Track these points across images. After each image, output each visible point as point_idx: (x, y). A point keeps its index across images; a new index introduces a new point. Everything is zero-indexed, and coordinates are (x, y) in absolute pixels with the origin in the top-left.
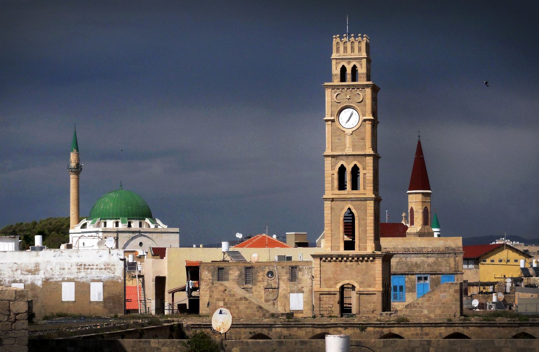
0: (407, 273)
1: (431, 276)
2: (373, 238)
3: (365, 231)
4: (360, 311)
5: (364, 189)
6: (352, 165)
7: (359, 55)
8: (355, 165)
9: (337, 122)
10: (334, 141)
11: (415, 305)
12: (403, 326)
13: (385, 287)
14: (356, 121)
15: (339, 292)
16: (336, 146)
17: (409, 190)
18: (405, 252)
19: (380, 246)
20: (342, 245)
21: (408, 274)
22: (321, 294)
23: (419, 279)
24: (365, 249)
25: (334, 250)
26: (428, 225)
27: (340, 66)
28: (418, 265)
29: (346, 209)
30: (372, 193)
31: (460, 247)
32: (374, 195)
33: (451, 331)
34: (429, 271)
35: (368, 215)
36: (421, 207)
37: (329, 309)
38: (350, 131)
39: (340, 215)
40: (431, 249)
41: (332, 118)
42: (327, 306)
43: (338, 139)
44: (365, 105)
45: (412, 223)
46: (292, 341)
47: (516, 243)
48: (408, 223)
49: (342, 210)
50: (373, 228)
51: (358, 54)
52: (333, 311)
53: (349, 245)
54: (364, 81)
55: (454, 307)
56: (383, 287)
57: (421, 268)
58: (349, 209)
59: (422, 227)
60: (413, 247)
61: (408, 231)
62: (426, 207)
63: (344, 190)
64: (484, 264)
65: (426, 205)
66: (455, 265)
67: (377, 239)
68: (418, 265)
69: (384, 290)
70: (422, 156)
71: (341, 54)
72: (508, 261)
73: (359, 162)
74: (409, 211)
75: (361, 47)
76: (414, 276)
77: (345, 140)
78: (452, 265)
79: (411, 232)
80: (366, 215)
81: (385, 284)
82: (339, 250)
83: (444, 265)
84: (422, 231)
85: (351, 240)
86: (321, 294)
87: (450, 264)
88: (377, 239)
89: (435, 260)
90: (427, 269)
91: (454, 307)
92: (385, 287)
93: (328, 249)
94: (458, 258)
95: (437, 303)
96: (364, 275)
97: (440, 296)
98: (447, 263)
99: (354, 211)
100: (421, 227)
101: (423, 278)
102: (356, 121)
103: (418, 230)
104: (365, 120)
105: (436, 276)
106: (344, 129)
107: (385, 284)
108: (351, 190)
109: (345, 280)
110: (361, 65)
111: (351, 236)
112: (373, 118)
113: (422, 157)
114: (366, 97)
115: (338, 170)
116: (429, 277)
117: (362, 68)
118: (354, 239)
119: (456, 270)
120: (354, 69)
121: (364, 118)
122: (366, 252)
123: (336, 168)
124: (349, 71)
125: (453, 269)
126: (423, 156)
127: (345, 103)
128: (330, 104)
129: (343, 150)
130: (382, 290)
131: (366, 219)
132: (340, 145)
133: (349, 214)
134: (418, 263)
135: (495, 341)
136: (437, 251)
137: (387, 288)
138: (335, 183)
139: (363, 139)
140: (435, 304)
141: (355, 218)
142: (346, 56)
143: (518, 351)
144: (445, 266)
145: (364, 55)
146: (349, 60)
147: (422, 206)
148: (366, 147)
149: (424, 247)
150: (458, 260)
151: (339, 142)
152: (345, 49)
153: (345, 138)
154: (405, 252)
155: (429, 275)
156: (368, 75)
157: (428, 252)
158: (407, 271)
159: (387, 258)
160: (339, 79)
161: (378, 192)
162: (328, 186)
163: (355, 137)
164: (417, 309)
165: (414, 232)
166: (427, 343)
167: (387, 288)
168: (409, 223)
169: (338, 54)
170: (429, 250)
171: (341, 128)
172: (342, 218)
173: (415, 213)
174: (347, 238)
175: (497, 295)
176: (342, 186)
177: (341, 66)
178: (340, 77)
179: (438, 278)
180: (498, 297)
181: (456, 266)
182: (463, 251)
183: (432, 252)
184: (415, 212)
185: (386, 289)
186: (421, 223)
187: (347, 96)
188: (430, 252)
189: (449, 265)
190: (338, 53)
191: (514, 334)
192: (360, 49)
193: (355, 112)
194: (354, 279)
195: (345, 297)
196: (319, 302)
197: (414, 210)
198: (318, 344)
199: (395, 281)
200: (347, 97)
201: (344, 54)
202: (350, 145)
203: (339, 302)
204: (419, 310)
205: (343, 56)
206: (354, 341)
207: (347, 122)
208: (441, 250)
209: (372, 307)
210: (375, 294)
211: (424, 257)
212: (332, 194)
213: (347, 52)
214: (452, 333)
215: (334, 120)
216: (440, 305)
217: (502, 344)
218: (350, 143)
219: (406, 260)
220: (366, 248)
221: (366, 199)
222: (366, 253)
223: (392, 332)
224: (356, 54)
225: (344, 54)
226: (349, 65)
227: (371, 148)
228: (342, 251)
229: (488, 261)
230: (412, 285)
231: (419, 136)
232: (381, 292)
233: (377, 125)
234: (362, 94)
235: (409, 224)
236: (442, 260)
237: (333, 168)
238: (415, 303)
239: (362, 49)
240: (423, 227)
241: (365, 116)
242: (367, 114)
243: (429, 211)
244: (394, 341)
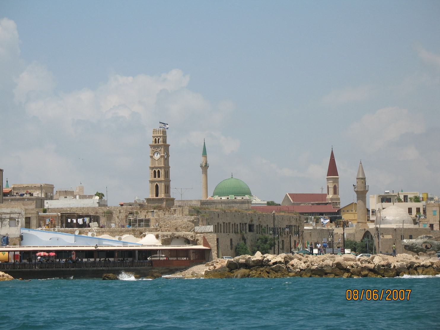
27: (155, 138)
124: (157, 140)
126: (334, 158)
139: (161, 162)
146: (157, 137)
176: (155, 177)
224: (159, 135)
228: (155, 197)
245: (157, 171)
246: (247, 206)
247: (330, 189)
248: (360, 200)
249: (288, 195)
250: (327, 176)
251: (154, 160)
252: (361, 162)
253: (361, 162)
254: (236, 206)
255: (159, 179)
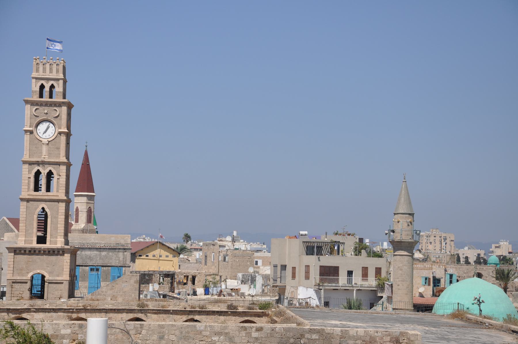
0: (82, 264)
1: (102, 268)
2: (63, 234)
3: (56, 229)
4: (49, 297)
5: (57, 191)
6: (47, 171)
7: (57, 76)
8: (50, 171)
9: (35, 133)
10: (31, 149)
11: (100, 293)
12: (435, 324)
13: (72, 277)
14: (52, 133)
15: (30, 281)
16: (33, 153)
17: (75, 192)
18: (81, 246)
19: (68, 241)
20: (35, 239)
21: (82, 266)
22: (13, 282)
23: (92, 270)
24: (56, 243)
25: (28, 244)
26: (91, 223)
27: (39, 84)
28: (91, 258)
29: (39, 209)
30: (64, 195)
31: (128, 244)
32: (66, 197)
33: (131, 316)
34: (101, 263)
35: (60, 214)
36: (85, 207)
37: (20, 295)
38: (45, 141)
39: (34, 213)
40: (103, 245)
41: (31, 129)
42: (18, 293)
43: (36, 147)
44: (61, 119)
45: (77, 221)
46: (22, 323)
47: (155, 240)
48: (73, 220)
49: (36, 209)
50: (63, 225)
51: (55, 75)
52: (23, 297)
53: (42, 240)
54: (61, 98)
55: (133, 295)
56: (70, 277)
57: (94, 261)
58: (43, 208)
59: (86, 224)
60: (88, 242)
61: (73, 228)
62: (90, 207)
63: (38, 192)
64: (140, 259)
65: (90, 205)
66: (123, 259)
67: (66, 236)
68: (91, 258)
69: (71, 279)
70: (88, 163)
71: (41, 74)
72: (160, 256)
73: (54, 168)
74: (75, 210)
75: (58, 69)
76: (87, 268)
77: (42, 148)
78: (121, 259)
79: (76, 229)
80: (58, 214)
81: (72, 274)
82: (32, 243)
83: (114, 259)
84: (86, 228)
85: (43, 235)
86: (13, 282)
87: (119, 258)
88: (66, 236)
89: (107, 254)
90: (100, 263)
91: (133, 295)
92: (72, 277)
93: (22, 242)
94: (126, 253)
95: (119, 292)
96: (54, 266)
97: (122, 286)
98: (117, 257)
99: (47, 210)
100: (84, 225)
101: (95, 270)
102: (52, 133)
103: (82, 227)
104: (60, 133)
105: (107, 268)
106: (41, 139)
107: (72, 274)
108: (45, 192)
109: (36, 270)
110: (58, 84)
111: (43, 232)
112: (67, 131)
113: (88, 164)
114: (62, 112)
115: (34, 174)
116: (102, 269)
117: (59, 87)
118: (46, 234)
119: (124, 263)
120: (52, 87)
121: (60, 130)
122: (31, 245)
123: (32, 172)
124: (47, 89)
125: (122, 263)
126: (89, 163)
127: (43, 117)
128: (29, 116)
129: (40, 157)
130: (69, 280)
131: (57, 218)
132: (37, 153)
133: (42, 212)
134: (92, 256)
135: (197, 325)
136: (109, 246)
137: (73, 278)
138: (31, 185)
139: (58, 148)
140: (117, 293)
141: (47, 216)
142: (45, 76)
143: (215, 334)
144: (115, 260)
145: (61, 76)
146: (48, 79)
147: (87, 206)
148: (61, 155)
149: (98, 243)
150: (126, 254)
151: (36, 150)
152: (51, 70)
153: (42, 147)
154: (81, 246)
155: (101, 267)
156: (64, 93)
157: (101, 247)
158: (82, 263)
159: (73, 253)
160: (38, 95)
161: (69, 194)
162: (24, 187)
163: (51, 147)
164: (101, 297)
165: (78, 229)
166: (140, 326)
167: (73, 278)
168: (75, 220)
169: (37, 74)
170: (102, 246)
171: (38, 138)
172: (36, 217)
173: (80, 213)
174: (40, 234)
175: (153, 285)
176: (37, 188)
177: (40, 84)
178: (39, 93)
179: (108, 269)
180: (154, 288)
181: (125, 260)
182: (131, 247)
183: (105, 247)
184: (81, 211)
185: (72, 278)
186: (85, 221)
187: (45, 111)
188: (103, 247)
189: (118, 258)
190: (38, 73)
191: (185, 319)
192: (57, 71)
193: (51, 125)
194: (44, 269)
195: (40, 285)
196: (11, 289)
197: (80, 210)
198: (45, 326)
199: (79, 271)
200: (45, 111)
201: (43, 74)
202: (46, 153)
203: (30, 289)
204: (103, 298)
205: (42, 75)
206: (77, 324)
207: (44, 134)
208: (112, 246)
209: (59, 294)
210: (62, 283)
211: (97, 251)
212: (28, 195)
213: (46, 73)
214: (132, 317)
215: (33, 130)
216: (121, 293)
217: (202, 328)
218: (46, 151)
219: (81, 253)
220: (57, 243)
221: (58, 201)
222: (56, 247)
223: (79, 316)
224: (54, 75)
225: (43, 74)
226: (47, 84)
227: (65, 157)
228: (35, 245)
229: (150, 255)
230: (86, 275)
231: (86, 146)
232: (68, 281)
233: (70, 137)
234: (59, 110)
235: (74, 222)
236: (112, 254)
237: (30, 172)
238: (100, 291)
239: (59, 71)
240: (87, 225)
241: (61, 129)
242: (62, 127)
243: (92, 211)
244: (112, 324)
245: (44, 172)
246: (90, 253)
247: (80, 215)
248: (393, 246)
249: (8, 221)
250: (76, 192)
251: (37, 141)
252: (405, 178)
253: (405, 178)
254: (223, 263)
255: (52, 194)
